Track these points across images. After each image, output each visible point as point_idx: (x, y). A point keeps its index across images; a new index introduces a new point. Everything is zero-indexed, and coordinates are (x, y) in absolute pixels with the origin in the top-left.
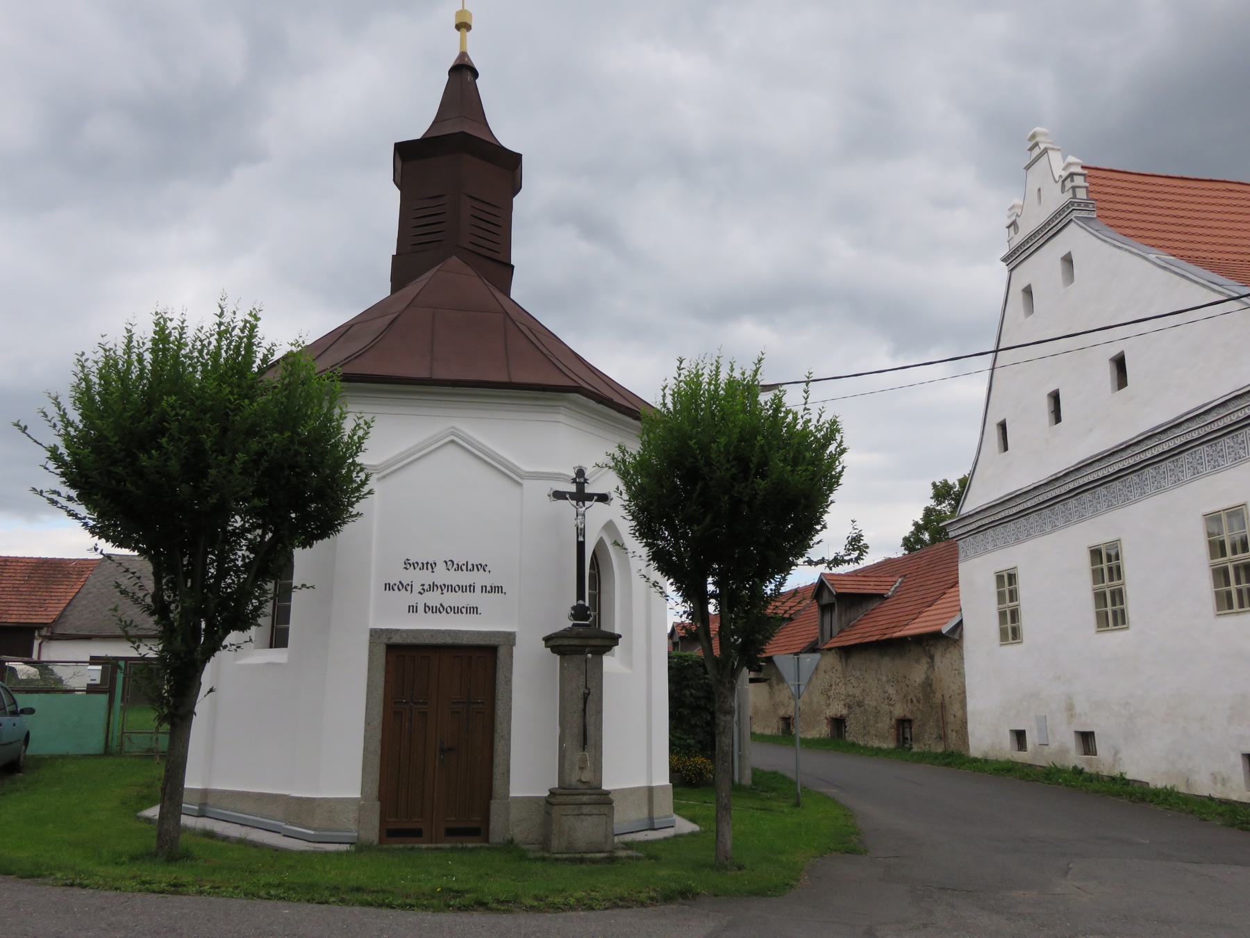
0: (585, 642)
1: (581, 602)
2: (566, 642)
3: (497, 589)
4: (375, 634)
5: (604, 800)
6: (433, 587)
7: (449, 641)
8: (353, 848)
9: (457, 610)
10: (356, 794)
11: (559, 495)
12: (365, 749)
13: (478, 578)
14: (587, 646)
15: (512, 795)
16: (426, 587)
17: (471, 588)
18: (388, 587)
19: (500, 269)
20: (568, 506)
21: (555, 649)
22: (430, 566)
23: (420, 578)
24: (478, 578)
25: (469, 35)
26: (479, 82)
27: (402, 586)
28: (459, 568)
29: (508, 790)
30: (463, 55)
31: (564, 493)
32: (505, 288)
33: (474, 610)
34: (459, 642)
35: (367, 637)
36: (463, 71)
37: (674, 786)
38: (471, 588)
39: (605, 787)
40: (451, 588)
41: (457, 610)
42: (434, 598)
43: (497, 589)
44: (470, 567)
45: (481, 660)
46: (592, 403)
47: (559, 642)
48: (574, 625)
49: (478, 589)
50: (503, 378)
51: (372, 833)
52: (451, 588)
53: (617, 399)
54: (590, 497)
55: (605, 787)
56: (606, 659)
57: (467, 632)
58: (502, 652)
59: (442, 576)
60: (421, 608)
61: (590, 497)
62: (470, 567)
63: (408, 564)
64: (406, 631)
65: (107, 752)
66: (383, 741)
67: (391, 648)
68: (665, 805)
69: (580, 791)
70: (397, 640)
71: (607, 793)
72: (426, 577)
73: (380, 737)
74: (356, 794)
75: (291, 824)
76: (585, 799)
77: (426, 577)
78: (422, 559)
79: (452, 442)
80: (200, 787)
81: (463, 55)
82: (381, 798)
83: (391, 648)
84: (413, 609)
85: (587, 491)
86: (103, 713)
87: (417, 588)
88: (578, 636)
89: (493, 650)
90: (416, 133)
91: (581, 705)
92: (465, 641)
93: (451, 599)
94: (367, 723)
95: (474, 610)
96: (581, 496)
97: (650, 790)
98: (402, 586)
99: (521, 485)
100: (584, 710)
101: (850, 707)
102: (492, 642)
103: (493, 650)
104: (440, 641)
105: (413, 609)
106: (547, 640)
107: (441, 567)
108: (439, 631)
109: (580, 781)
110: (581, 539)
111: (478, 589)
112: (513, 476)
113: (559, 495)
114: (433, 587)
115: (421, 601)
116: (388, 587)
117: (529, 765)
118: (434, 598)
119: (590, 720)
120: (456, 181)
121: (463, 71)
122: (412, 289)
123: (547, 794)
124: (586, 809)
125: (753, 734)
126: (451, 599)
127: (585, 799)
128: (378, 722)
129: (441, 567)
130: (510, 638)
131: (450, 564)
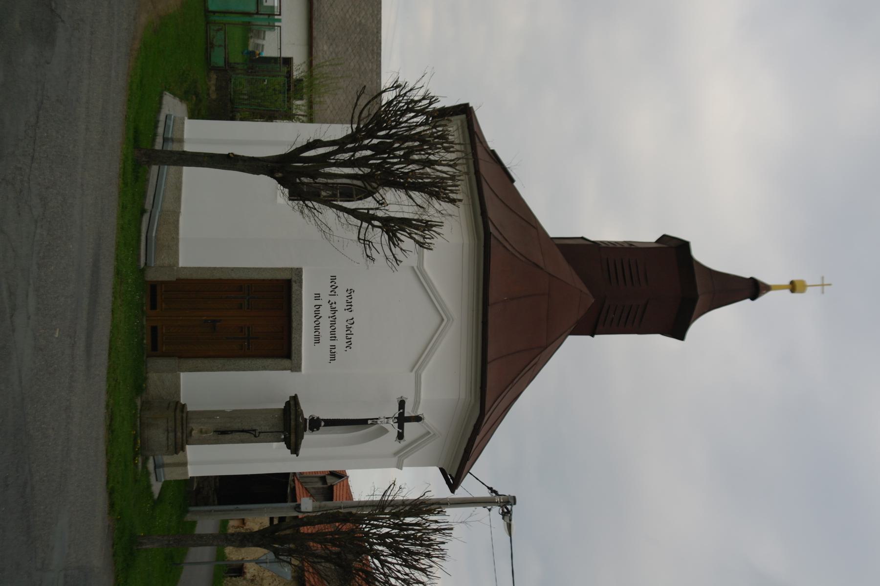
0: (293, 430)
1: (323, 424)
2: (293, 412)
3: (333, 357)
4: (299, 272)
5: (179, 448)
6: (334, 310)
7: (294, 324)
8: (142, 265)
9: (317, 328)
10: (181, 264)
11: (402, 404)
12: (215, 268)
13: (341, 342)
14: (290, 434)
15: (182, 375)
16: (334, 306)
17: (333, 338)
18: (333, 279)
19: (593, 325)
20: (395, 411)
21: (288, 403)
22: (349, 307)
23: (341, 301)
24: (341, 342)
25: (787, 292)
26: (748, 301)
27: (334, 288)
28: (348, 329)
29: (185, 371)
30: (768, 288)
31: (403, 409)
32: (578, 331)
33: (317, 340)
34: (294, 331)
35: (295, 265)
36: (753, 289)
37: (186, 481)
38: (333, 338)
39: (188, 447)
40: (333, 323)
41: (317, 328)
42: (325, 311)
43: (333, 357)
44: (349, 336)
45: (280, 347)
46: (474, 422)
47: (293, 408)
48: (306, 419)
49: (333, 343)
50: (491, 354)
51: (152, 276)
52: (333, 323)
53: (478, 438)
54: (401, 427)
55: (188, 447)
56: (283, 444)
57: (301, 337)
58: (286, 362)
59: (342, 317)
60: (318, 302)
61: (401, 427)
62: (349, 336)
63: (350, 292)
64: (301, 293)
65: (207, 12)
66: (221, 280)
67: (288, 283)
68: (172, 474)
69: (184, 426)
70: (295, 287)
71: (183, 449)
72: (341, 305)
73: (223, 277)
74: (181, 264)
75: (160, 216)
76: (179, 434)
77: (341, 305)
78: (354, 302)
79: (443, 320)
80: (185, 137)
81: (768, 288)
82: (179, 281)
83: (288, 283)
84: (317, 297)
85: (406, 424)
86: (241, 8)
87: (333, 299)
88: (296, 420)
89: (288, 356)
90: (699, 254)
91: (246, 428)
92: (294, 335)
93: (325, 323)
94: (233, 269)
95: (317, 340)
96: (402, 420)
97: (185, 464)
98: (334, 288)
99: (411, 371)
100: (243, 431)
101: (252, 580)
102: (294, 356)
103: (288, 356)
104: (294, 318)
105: (317, 297)
106: (295, 398)
107: (349, 315)
108: (301, 317)
109: (192, 430)
110: (370, 422)
111: (333, 343)
112: (417, 366)
113: (402, 404)
114: (334, 310)
115: (324, 302)
116: (333, 279)
117: (204, 387)
118: (325, 311)
119: (237, 436)
120: (659, 288)
121: (753, 289)
122: (565, 272)
123: (182, 401)
124: (171, 435)
125: (227, 521)
126: (325, 323)
127: (179, 434)
128: (235, 276)
129: (349, 315)
130: (297, 368)
131: (352, 321)
